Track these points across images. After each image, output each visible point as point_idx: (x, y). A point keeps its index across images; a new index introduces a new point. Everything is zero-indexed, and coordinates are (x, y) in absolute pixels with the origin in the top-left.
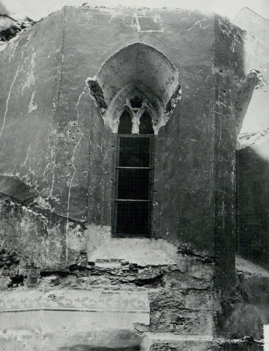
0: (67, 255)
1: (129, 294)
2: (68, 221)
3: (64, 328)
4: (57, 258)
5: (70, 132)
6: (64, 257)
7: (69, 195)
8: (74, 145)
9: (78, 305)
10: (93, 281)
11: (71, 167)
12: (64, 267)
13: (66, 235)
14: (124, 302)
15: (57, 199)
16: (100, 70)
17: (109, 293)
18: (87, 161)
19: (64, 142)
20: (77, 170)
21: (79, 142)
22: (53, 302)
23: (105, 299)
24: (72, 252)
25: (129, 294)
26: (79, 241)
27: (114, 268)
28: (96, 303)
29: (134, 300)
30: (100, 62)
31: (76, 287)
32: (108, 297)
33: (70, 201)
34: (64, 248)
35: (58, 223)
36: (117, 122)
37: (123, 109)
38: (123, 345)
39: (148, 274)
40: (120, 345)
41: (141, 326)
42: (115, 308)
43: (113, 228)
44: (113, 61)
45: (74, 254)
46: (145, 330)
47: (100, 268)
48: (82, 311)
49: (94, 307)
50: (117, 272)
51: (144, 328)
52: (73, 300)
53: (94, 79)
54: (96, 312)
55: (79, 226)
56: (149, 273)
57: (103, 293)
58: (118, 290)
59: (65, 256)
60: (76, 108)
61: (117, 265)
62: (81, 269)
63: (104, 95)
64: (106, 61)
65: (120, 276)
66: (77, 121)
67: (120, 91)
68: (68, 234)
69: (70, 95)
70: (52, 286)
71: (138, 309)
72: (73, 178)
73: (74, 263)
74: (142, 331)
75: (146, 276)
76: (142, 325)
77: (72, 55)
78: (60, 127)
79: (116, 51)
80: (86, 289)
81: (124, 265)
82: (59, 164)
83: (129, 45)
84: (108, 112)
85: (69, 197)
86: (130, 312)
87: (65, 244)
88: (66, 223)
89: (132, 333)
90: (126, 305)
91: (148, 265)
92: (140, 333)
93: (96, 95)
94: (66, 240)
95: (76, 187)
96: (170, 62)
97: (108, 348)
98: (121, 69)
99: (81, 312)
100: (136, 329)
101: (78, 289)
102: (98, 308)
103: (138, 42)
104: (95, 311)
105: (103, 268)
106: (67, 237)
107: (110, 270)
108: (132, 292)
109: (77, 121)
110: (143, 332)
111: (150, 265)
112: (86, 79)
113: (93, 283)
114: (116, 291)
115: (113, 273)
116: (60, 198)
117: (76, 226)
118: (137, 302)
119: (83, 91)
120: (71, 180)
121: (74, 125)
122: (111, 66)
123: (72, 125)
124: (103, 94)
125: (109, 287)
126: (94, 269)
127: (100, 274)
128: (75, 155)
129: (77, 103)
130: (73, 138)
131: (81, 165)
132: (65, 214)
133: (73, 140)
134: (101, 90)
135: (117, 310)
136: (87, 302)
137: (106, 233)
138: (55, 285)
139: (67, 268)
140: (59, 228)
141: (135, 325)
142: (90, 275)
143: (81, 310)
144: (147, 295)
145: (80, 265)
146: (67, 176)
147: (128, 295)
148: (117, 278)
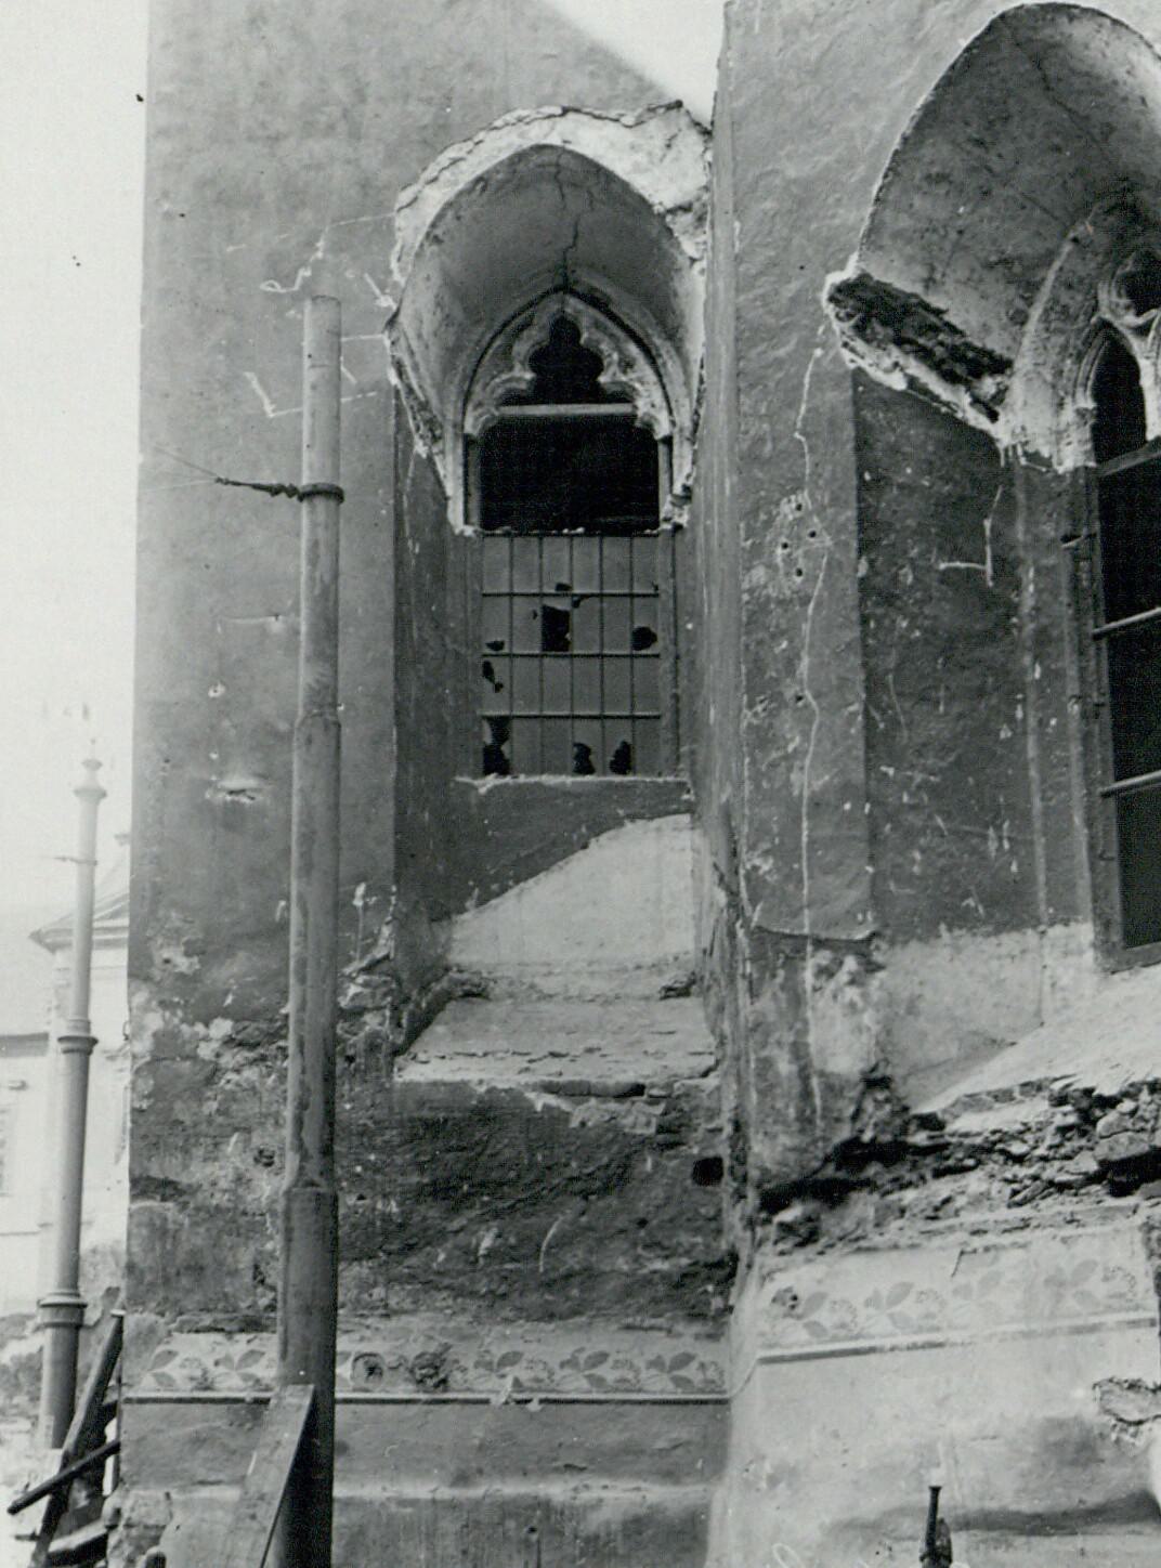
0: (818, 1101)
1: (1064, 1240)
2: (809, 948)
3: (836, 1435)
4: (785, 1123)
5: (787, 551)
6: (808, 1112)
7: (805, 833)
8: (805, 601)
9: (878, 1328)
10: (937, 1200)
11: (800, 704)
12: (816, 1158)
13: (809, 1014)
14: (1047, 1282)
15: (766, 861)
16: (867, 222)
17: (987, 1249)
18: (852, 658)
19: (768, 598)
20: (822, 709)
21: (820, 584)
22: (790, 1321)
23: (974, 1280)
24: (833, 1089)
25: (1064, 1240)
26: (852, 1032)
27: (1025, 1124)
28: (943, 1304)
29: (1088, 1267)
30: (867, 181)
31: (863, 1243)
32: (982, 1272)
33: (809, 859)
34: (804, 1075)
35: (775, 968)
36: (1081, 413)
37: (1097, 342)
38: (1084, 1497)
39: (1138, 1127)
40: (1069, 1497)
41: (1131, 1395)
42: (1012, 1320)
43: (1105, 925)
44: (927, 152)
45: (842, 1089)
46: (1147, 1410)
47: (966, 1135)
48: (893, 1349)
49: (935, 1322)
50: (1031, 1143)
51: (1145, 1404)
52: (858, 1302)
53: (849, 273)
54: (947, 1349)
55: (851, 963)
56: (1142, 1124)
57: (962, 1253)
58: (1022, 1228)
59: (814, 1111)
60: (797, 435)
61: (1035, 1110)
62: (893, 1153)
63: (952, 318)
64: (883, 170)
65: (1044, 1159)
66: (806, 493)
67: (1057, 265)
68: (813, 1008)
69: (772, 385)
70: (782, 1253)
71: (1109, 1309)
72: (811, 749)
73: (844, 1133)
74: (1136, 1416)
75: (1131, 1140)
76: (1134, 1386)
77: (768, 205)
78: (749, 542)
79: (920, 102)
80: (896, 1247)
81: (1060, 1100)
82: (759, 708)
83: (964, 43)
84: (1017, 386)
85: (805, 839)
86: (1078, 1330)
87: (808, 1055)
88: (803, 959)
89: (1096, 1432)
90: (1059, 1298)
91: (1132, 1085)
92: (1132, 1429)
93: (910, 334)
94: (811, 1039)
95: (825, 789)
96: (1141, 37)
97: (1018, 1513)
98: (997, 166)
99: (890, 1354)
100: (1108, 1412)
101: (869, 1250)
102: (951, 1327)
103: (999, 11)
104: (940, 1345)
105: (979, 1134)
106: (812, 1022)
107: (1006, 1137)
108: (1080, 1231)
109: (806, 493)
110: (1140, 1423)
111: (1144, 1083)
112: (820, 288)
113: (941, 1214)
114: (1018, 1237)
115: (1017, 1148)
116: (775, 856)
117: (841, 963)
118: (1101, 1275)
119: (817, 346)
120: (807, 762)
121: (798, 514)
122: (928, 177)
123: (791, 517)
124: (946, 318)
125: (985, 1222)
126: (949, 1144)
127: (970, 1162)
128: (812, 646)
129: (798, 413)
130: (799, 573)
131: (835, 682)
132: (796, 921)
133: (799, 580)
134: (927, 307)
135: (1023, 1327)
136: (910, 1308)
137: (1071, 960)
138: (802, 1245)
139: (827, 1160)
140: (783, 987)
141: (1104, 1393)
142: (928, 1176)
143: (888, 1343)
144: (1139, 1236)
145: (874, 1140)
146: (790, 748)
147: (1061, 1248)
148: (1032, 1171)
